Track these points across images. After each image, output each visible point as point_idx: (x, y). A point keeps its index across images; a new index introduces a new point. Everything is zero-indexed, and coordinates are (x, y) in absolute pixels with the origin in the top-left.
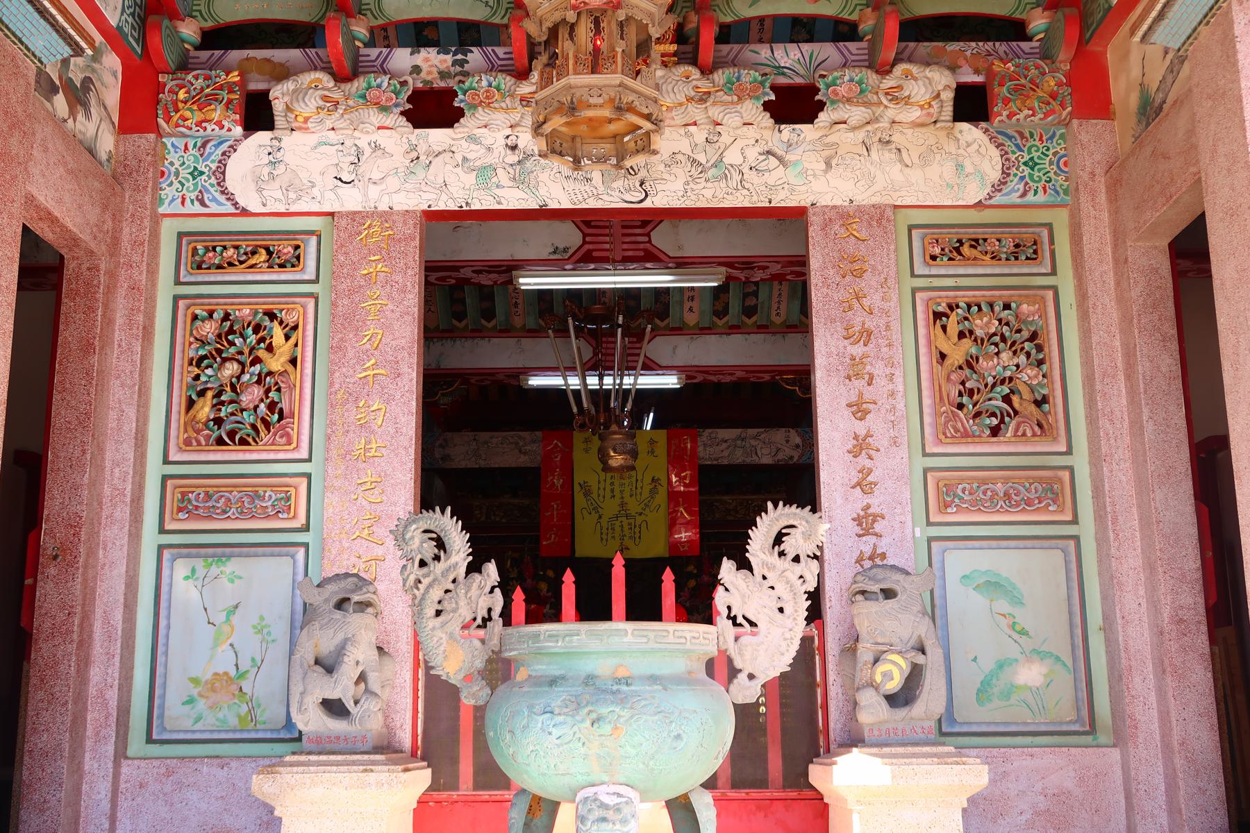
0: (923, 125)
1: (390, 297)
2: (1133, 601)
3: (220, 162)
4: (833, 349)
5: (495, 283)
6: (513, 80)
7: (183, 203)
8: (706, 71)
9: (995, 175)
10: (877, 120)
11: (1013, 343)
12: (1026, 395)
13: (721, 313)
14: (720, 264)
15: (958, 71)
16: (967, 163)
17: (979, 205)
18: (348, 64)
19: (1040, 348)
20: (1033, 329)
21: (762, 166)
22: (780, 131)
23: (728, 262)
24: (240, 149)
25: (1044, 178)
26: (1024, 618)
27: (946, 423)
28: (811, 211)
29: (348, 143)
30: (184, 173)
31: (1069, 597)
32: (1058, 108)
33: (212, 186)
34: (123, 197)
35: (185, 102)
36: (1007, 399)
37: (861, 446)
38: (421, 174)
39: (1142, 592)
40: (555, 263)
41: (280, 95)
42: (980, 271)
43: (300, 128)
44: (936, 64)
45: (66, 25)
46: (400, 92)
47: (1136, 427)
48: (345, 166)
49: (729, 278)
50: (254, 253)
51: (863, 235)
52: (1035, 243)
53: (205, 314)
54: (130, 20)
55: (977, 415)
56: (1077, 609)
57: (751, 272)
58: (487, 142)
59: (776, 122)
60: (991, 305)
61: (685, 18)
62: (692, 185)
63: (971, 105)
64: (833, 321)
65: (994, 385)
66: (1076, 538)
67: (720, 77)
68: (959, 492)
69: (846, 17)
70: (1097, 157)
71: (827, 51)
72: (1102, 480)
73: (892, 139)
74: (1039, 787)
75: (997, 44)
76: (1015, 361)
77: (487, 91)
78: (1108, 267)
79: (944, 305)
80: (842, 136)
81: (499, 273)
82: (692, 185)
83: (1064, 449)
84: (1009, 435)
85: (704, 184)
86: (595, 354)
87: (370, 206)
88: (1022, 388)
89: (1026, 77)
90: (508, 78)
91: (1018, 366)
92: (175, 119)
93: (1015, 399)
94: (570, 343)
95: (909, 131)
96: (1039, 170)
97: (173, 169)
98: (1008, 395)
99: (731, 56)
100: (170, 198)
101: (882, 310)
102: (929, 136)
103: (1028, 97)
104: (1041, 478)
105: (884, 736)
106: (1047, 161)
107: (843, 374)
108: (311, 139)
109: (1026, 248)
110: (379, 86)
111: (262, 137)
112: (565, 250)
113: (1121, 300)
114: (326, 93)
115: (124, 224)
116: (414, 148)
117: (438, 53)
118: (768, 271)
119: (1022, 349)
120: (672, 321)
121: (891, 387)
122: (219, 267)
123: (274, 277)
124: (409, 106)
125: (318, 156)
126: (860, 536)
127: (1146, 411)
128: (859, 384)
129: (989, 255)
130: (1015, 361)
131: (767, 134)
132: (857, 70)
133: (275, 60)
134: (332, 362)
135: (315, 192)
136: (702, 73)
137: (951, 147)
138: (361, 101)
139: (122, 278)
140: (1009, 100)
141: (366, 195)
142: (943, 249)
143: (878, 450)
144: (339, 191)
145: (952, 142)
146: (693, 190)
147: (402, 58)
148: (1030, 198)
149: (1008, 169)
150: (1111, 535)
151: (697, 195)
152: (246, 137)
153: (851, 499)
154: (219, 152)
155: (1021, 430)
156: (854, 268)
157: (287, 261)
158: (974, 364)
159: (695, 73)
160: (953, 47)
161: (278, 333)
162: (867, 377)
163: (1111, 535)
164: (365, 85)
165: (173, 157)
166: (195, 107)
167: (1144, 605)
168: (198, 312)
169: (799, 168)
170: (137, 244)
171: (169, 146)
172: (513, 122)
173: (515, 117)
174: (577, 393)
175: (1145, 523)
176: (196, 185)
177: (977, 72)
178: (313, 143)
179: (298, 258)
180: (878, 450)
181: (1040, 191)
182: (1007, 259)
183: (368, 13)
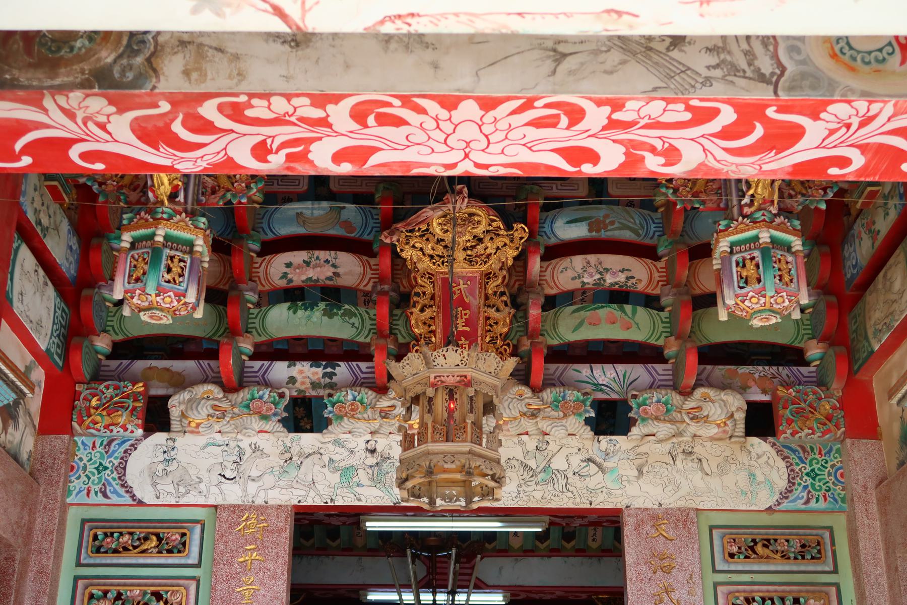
0: (720, 439)
1: (262, 583)
3: (122, 458)
5: (344, 524)
6: (374, 394)
7: (88, 495)
8: (536, 390)
9: (782, 484)
15: (748, 390)
16: (758, 473)
17: (769, 509)
18: (235, 379)
21: (584, 472)
22: (599, 442)
24: (140, 447)
25: (824, 487)
28: (626, 512)
29: (232, 444)
30: (91, 468)
32: (833, 428)
33: (114, 479)
34: (38, 491)
35: (96, 408)
38: (293, 473)
41: (176, 406)
42: (772, 568)
43: (192, 432)
44: (730, 388)
45: (15, 379)
48: (228, 464)
49: (551, 524)
50: (146, 539)
51: (671, 534)
52: (819, 544)
53: (100, 593)
54: (56, 341)
58: (351, 446)
59: (596, 434)
61: (518, 341)
62: (524, 487)
63: (760, 421)
67: (548, 395)
69: (653, 342)
70: (869, 472)
71: (637, 372)
73: (695, 450)
75: (781, 368)
77: (352, 404)
78: (882, 570)
79: (742, 598)
82: (524, 487)
90: (370, 392)
92: (87, 423)
94: (407, 562)
95: (708, 444)
96: (820, 480)
97: (81, 464)
99: (558, 374)
100: (77, 490)
102: (726, 448)
103: (807, 418)
106: (826, 473)
108: (201, 440)
110: (261, 398)
111: (159, 438)
114: (216, 403)
115: (38, 515)
116: (288, 450)
117: (311, 366)
118: (586, 520)
122: (115, 551)
123: (162, 561)
124: (285, 415)
129: (779, 554)
131: (588, 444)
132: (663, 392)
133: (174, 369)
135: (202, 487)
136: (533, 391)
137: (745, 459)
138: (245, 410)
139: (32, 564)
140: (792, 421)
141: (245, 490)
142: (739, 548)
144: (223, 487)
145: (744, 454)
146: (525, 492)
147: (280, 370)
148: (813, 505)
149: (793, 478)
151: (529, 496)
152: (145, 437)
154: (122, 450)
156: (663, 564)
157: (174, 547)
159: (527, 392)
160: (743, 370)
164: (249, 396)
165: (82, 453)
166: (105, 413)
168: (94, 591)
170: (47, 532)
171: (80, 444)
172: (373, 430)
173: (375, 425)
176: (100, 479)
177: (764, 392)
179: (184, 544)
181: (821, 499)
182: (795, 558)
183: (254, 330)
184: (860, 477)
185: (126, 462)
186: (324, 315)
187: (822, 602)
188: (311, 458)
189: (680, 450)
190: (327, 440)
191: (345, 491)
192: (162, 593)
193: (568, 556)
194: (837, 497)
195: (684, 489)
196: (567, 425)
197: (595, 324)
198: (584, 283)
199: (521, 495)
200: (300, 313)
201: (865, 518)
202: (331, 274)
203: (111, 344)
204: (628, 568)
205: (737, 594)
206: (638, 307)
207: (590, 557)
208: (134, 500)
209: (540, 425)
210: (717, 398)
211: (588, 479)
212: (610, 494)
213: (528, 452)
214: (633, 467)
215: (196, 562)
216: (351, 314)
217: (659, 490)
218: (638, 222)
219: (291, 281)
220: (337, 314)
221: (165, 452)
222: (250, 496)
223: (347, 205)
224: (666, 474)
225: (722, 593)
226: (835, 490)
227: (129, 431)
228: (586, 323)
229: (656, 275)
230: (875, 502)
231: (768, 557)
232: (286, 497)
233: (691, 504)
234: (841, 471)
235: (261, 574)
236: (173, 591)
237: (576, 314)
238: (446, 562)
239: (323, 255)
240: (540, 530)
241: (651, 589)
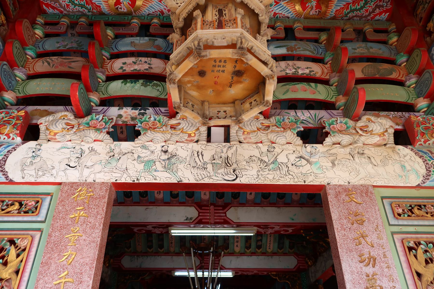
0: (379, 146)
1: (84, 232)
3: (5, 155)
4: (354, 269)
6: (168, 119)
9: (423, 171)
10: (355, 142)
13: (248, 247)
14: (255, 226)
16: (406, 165)
21: (298, 164)
22: (306, 147)
23: (258, 225)
24: (18, 149)
29: (77, 148)
38: (114, 163)
40: (187, 224)
41: (43, 123)
42: (426, 223)
46: (107, 122)
48: (73, 159)
50: (12, 204)
51: (359, 200)
57: (267, 230)
58: (152, 149)
62: (261, 172)
63: (403, 138)
64: (351, 251)
69: (329, 100)
73: (365, 152)
75: (404, 113)
77: (153, 122)
79: (412, 242)
80: (337, 150)
81: (163, 228)
82: (261, 172)
85: (268, 172)
86: (201, 263)
87: (83, 180)
89: (429, 123)
95: (373, 149)
101: (379, 245)
108: (59, 145)
110: (97, 119)
111: (32, 144)
112: (191, 219)
116: (112, 151)
118: (274, 230)
120: (230, 250)
124: (111, 130)
125: (60, 154)
131: (299, 148)
134: (40, 273)
135: (54, 172)
141: (82, 174)
142: (403, 210)
144: (67, 172)
146: (262, 175)
149: (429, 168)
152: (23, 144)
154: (6, 150)
156: (358, 220)
157: (30, 209)
161: (13, 252)
172: (166, 139)
174: (193, 279)
178: (58, 148)
179: (36, 208)
183: (101, 93)
185: (7, 157)
186: (142, 86)
188: (126, 155)
189: (356, 152)
190: (138, 145)
191: (147, 174)
192: (15, 239)
193: (259, 256)
195: (363, 174)
196: (287, 135)
197: (295, 91)
198: (287, 73)
199: (260, 177)
200: (128, 85)
202: (148, 68)
203: (15, 98)
204: (334, 222)
205: (409, 239)
206: (318, 84)
207: (268, 256)
208: (7, 180)
209: (269, 137)
210: (376, 121)
211: (301, 168)
212: (316, 176)
213: (262, 153)
214: (329, 161)
215: (43, 219)
216: (157, 85)
217: (347, 174)
218: (312, 48)
219: (125, 70)
220: (149, 85)
221: (33, 152)
222: (85, 177)
223: (158, 39)
224: (350, 165)
225: (397, 239)
227: (11, 138)
228: (290, 91)
229: (326, 71)
231: (422, 216)
232: (108, 178)
233: (368, 183)
235: (85, 225)
236: (23, 238)
237: (284, 87)
238: (208, 258)
239: (144, 59)
240: (252, 235)
241: (352, 235)
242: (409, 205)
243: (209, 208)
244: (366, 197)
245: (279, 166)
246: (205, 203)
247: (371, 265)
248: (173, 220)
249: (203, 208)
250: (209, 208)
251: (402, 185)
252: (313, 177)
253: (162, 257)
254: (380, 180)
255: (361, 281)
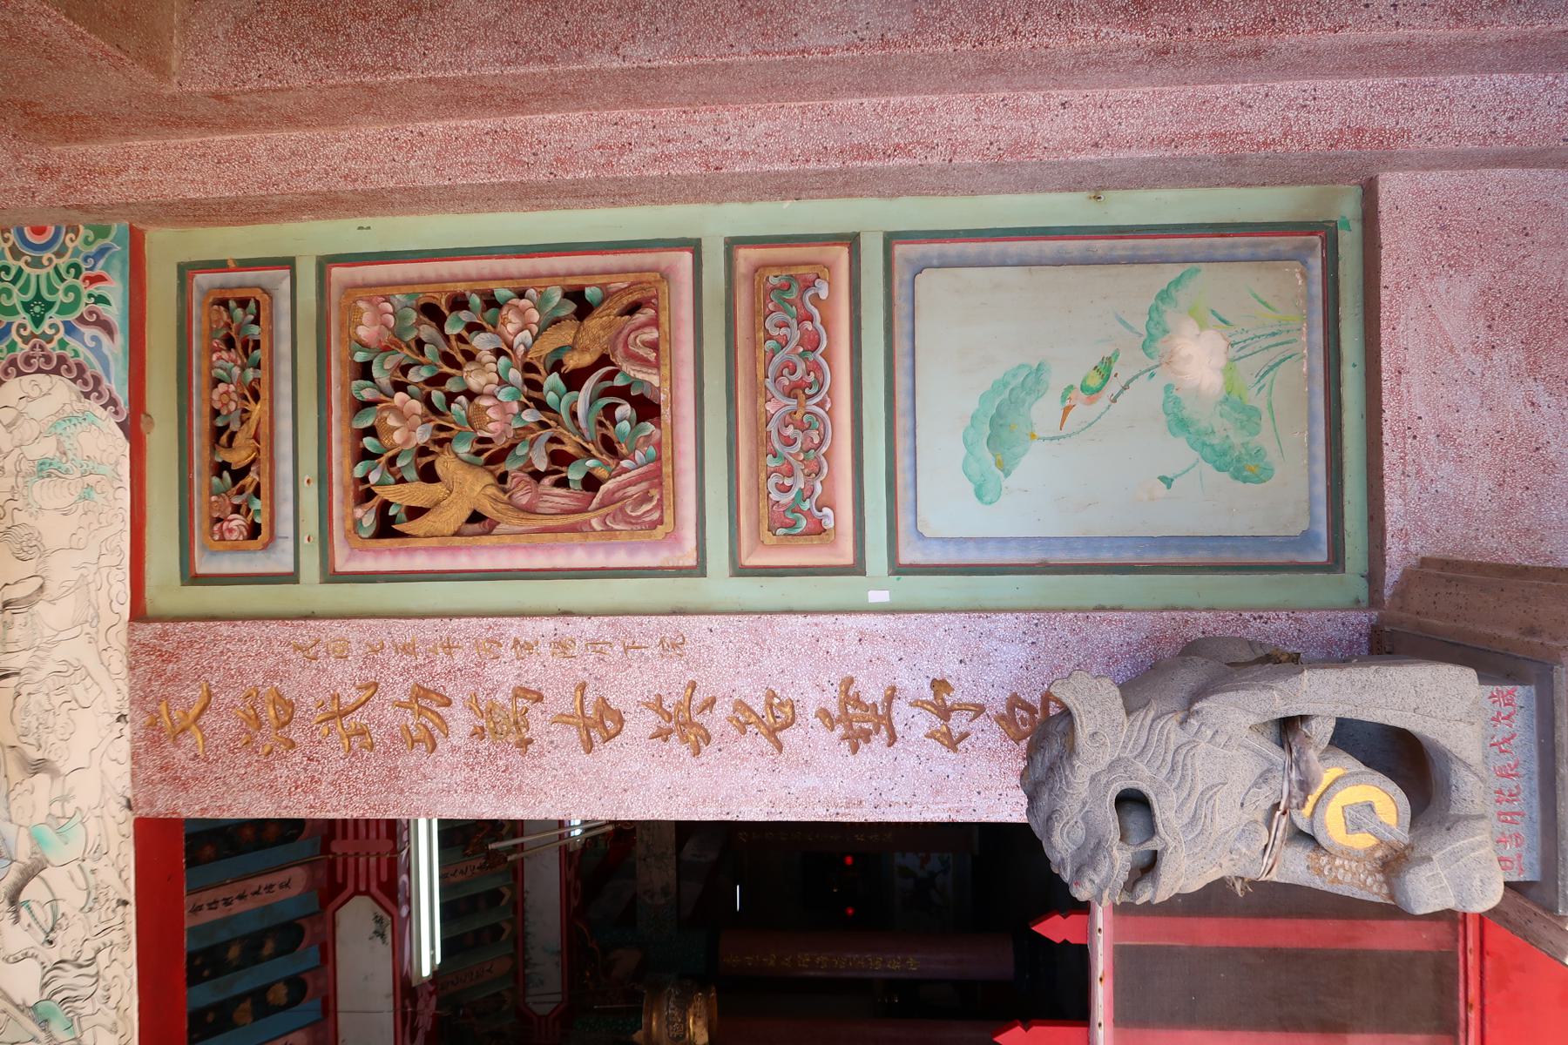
2: (1055, 118)
4: (458, 777)
9: (61, 391)
11: (448, 359)
12: (564, 335)
17: (134, 430)
19: (459, 303)
20: (414, 315)
25: (70, 280)
26: (1072, 367)
27: (628, 520)
28: (144, 812)
31: (1022, 263)
36: (574, 381)
37: (683, 724)
39: (1035, 99)
40: (397, 929)
47: (639, 88)
51: (195, 694)
52: (224, 303)
55: (609, 446)
56: (1050, 247)
60: (362, 406)
64: (394, 773)
65: (542, 406)
66: (891, 239)
68: (785, 499)
72: (764, 177)
74: (1471, 361)
76: (487, 357)
78: (258, 143)
79: (359, 512)
83: (687, 257)
84: (655, 380)
88: (548, 344)
91: (498, 353)
93: (573, 362)
96: (52, 290)
98: (563, 377)
101: (369, 660)
104: (754, 313)
105: (1521, 828)
106: (33, 272)
107: (515, 758)
109: (235, 323)
112: (378, 920)
113: (327, 114)
119: (460, 338)
121: (545, 649)
126: (892, 739)
127: (596, 62)
128: (538, 722)
129: (252, 406)
130: (487, 357)
142: (237, 509)
143: (693, 686)
148: (115, 312)
149: (48, 359)
150: (899, 161)
153: (806, 754)
155: (643, 352)
156: (270, 722)
158: (494, 448)
162: (522, 703)
163: (899, 161)
167: (1065, 94)
169: (48, 833)
175: (876, 79)
180: (693, 686)
184: (18, 183)
187: (362, 305)
194: (94, 249)
195: (78, 650)
201: (123, 178)
204: (285, 814)
211: (62, 907)
214: (28, 783)
224: (43, 699)
225: (348, 560)
226: (76, 253)
230: (82, 148)
234: (27, 231)
241: (334, 757)
242: (216, 480)
243: (340, 861)
244: (181, 664)
245: (58, 997)
246: (321, 874)
247: (443, 711)
248: (384, 982)
249: (340, 879)
250: (340, 861)
251: (125, 496)
252: (99, 865)
253: (526, 886)
254: (106, 586)
255: (500, 763)
